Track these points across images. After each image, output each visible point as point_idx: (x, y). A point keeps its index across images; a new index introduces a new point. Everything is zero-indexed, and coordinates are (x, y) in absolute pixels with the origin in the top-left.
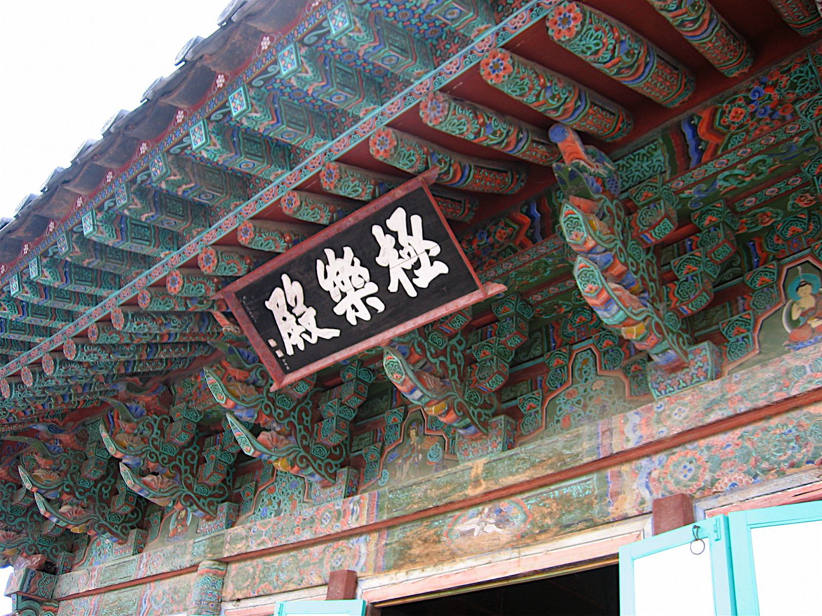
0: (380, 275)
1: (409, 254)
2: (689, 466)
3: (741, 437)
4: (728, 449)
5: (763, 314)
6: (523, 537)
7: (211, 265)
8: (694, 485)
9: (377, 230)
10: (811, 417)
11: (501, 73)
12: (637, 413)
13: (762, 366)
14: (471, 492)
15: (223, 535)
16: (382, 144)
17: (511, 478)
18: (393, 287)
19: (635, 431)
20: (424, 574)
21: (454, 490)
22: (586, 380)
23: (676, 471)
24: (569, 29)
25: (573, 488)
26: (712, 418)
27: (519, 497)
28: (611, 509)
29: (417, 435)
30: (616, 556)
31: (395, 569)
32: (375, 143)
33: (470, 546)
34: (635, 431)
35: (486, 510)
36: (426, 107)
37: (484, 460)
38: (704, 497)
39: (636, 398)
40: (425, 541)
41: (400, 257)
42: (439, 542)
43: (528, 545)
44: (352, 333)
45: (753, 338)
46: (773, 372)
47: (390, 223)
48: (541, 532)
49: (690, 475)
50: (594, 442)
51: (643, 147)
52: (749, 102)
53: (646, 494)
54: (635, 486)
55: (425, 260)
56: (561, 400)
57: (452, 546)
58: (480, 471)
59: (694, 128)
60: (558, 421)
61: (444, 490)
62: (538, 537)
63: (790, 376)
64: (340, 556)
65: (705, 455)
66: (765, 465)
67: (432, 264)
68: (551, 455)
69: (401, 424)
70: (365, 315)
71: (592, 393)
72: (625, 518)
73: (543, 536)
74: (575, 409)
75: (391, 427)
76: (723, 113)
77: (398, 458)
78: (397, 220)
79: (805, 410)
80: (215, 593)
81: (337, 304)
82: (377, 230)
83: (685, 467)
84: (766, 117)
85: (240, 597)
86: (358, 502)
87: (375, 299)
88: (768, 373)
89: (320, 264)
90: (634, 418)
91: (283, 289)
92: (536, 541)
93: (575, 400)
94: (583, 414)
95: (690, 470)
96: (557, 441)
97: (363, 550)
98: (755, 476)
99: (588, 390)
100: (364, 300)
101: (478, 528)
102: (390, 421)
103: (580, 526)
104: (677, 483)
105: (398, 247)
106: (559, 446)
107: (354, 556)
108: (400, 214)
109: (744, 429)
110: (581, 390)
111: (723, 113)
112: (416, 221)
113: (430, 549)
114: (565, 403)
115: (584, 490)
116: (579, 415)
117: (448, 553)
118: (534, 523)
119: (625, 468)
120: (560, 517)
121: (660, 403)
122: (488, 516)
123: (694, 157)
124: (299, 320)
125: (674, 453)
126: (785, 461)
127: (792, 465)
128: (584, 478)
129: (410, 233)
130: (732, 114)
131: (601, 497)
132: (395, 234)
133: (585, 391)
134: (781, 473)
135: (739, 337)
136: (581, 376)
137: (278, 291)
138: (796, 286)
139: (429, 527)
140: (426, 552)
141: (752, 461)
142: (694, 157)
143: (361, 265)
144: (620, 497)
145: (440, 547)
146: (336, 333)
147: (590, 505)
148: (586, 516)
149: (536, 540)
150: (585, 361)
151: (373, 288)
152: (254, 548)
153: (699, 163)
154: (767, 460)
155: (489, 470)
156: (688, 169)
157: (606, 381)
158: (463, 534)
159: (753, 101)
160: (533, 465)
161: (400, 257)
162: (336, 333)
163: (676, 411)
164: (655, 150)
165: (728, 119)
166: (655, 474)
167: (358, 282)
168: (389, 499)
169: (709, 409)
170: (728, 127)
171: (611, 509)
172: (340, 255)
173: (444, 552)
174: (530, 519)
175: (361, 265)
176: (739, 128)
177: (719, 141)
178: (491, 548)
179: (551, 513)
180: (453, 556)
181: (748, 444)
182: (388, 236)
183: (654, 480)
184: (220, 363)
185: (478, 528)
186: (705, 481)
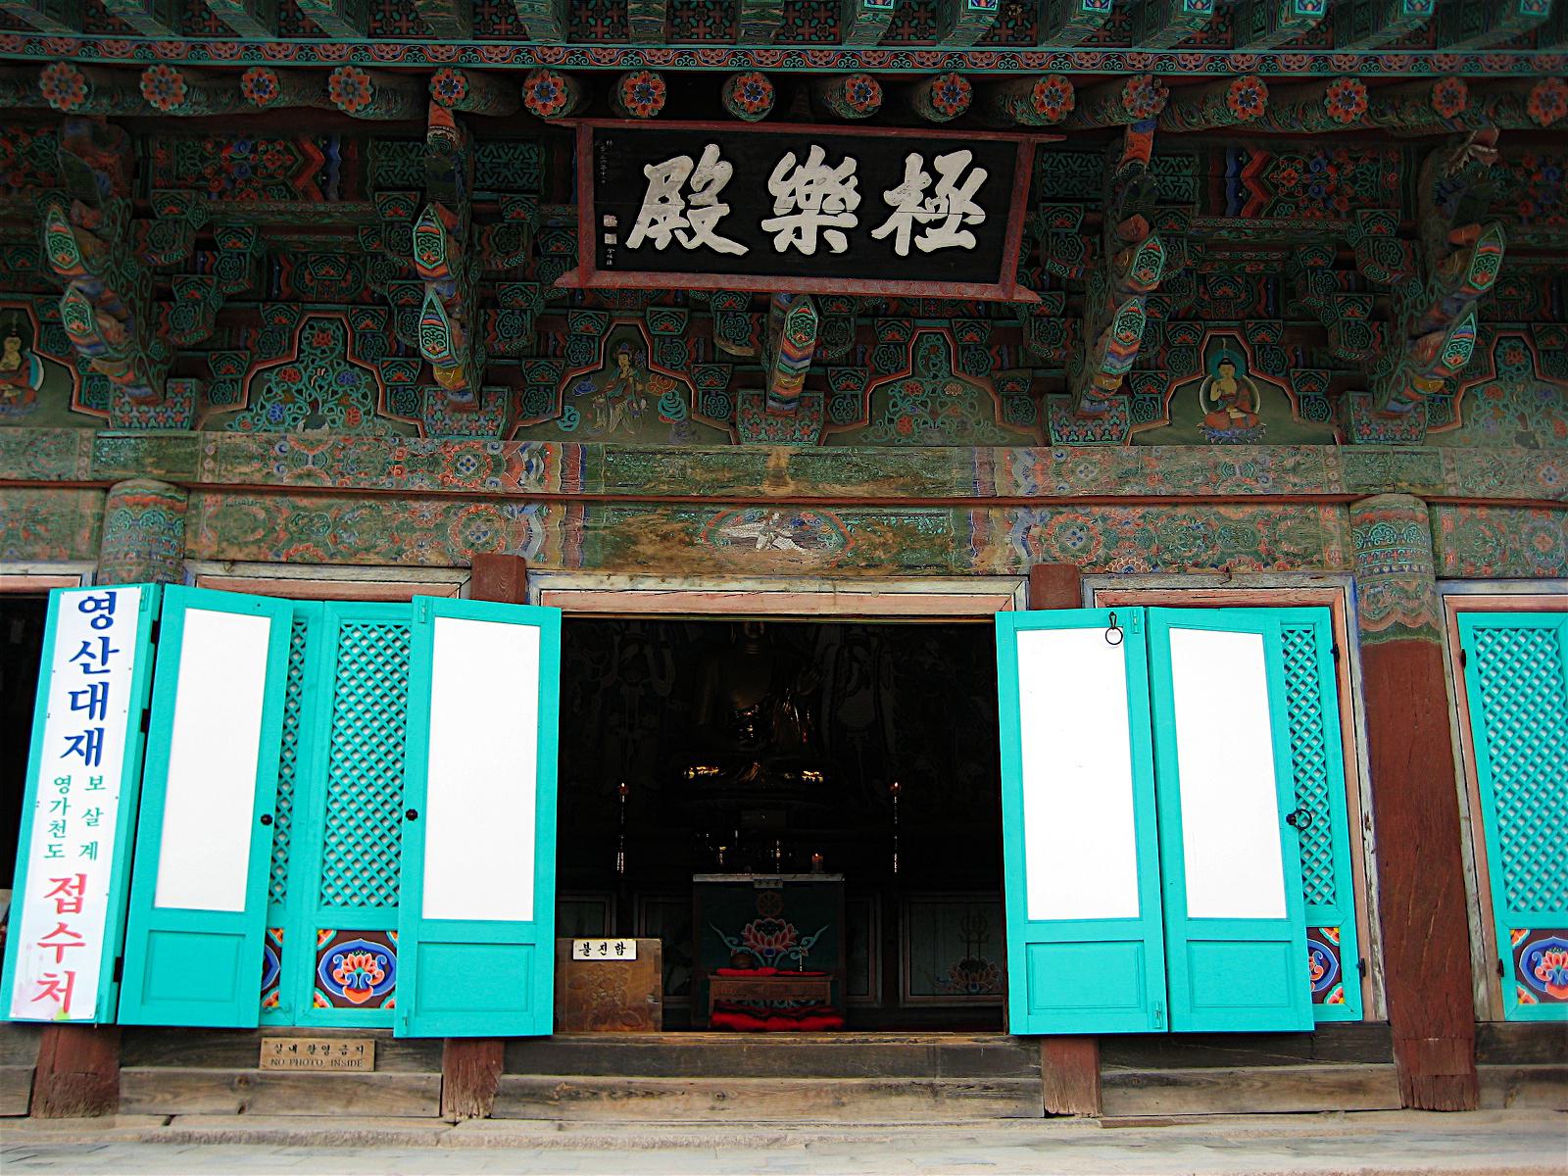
0: (873, 211)
1: (937, 208)
2: (1079, 534)
3: (1143, 517)
4: (1127, 527)
5: (1180, 379)
6: (840, 566)
7: (650, 105)
8: (1085, 558)
9: (914, 161)
10: (1220, 518)
11: (1250, 110)
12: (1029, 454)
13: (1188, 449)
14: (767, 489)
15: (195, 440)
16: (1051, 97)
17: (838, 487)
18: (879, 233)
19: (1027, 477)
20: (665, 586)
21: (737, 479)
22: (935, 376)
23: (1067, 537)
24: (1347, 112)
25: (921, 519)
26: (1127, 490)
27: (833, 512)
28: (973, 560)
29: (632, 365)
30: (992, 617)
31: (607, 568)
32: (1042, 92)
33: (749, 561)
34: (1027, 477)
35: (776, 516)
36: (1136, 88)
37: (792, 448)
38: (1093, 573)
39: (1007, 426)
40: (665, 537)
41: (922, 204)
42: (693, 544)
43: (846, 579)
44: (763, 257)
45: (1163, 404)
46: (1200, 460)
47: (940, 162)
48: (868, 566)
49: (1080, 544)
50: (967, 473)
51: (1174, 156)
52: (1307, 170)
53: (1022, 553)
54: (1007, 540)
55: (954, 222)
56: (896, 391)
57: (717, 555)
58: (783, 463)
59: (1240, 166)
60: (891, 421)
61: (719, 476)
62: (864, 572)
63: (1219, 472)
64: (484, 528)
65: (1100, 526)
66: (1167, 557)
67: (958, 231)
68: (902, 472)
69: (601, 338)
70: (808, 246)
71: (944, 398)
72: (992, 575)
73: (872, 572)
74: (918, 411)
75: (579, 338)
76: (1277, 167)
77: (598, 393)
78: (951, 164)
79: (1215, 509)
80: (174, 542)
81: (774, 216)
82: (914, 161)
83: (1074, 533)
84: (1319, 198)
85: (240, 556)
86: (541, 452)
87: (842, 236)
88: (1194, 458)
89: (790, 159)
90: (1024, 458)
91: (696, 163)
92: (860, 577)
93: (920, 399)
94: (931, 423)
95: (1080, 539)
96: (911, 456)
97: (537, 527)
98: (1155, 566)
99: (939, 391)
100: (821, 229)
101: (762, 540)
102: (580, 327)
103: (928, 571)
104: (1064, 550)
105: (929, 192)
106: (916, 462)
107: (519, 534)
108: (964, 157)
109: (1147, 509)
110: (929, 388)
111: (1277, 167)
112: (979, 176)
113: (674, 552)
114: (903, 398)
115: (937, 527)
116: (925, 423)
117: (711, 563)
118: (857, 552)
119: (994, 513)
120: (899, 553)
121: (1061, 451)
122: (779, 524)
123: (1232, 204)
124: (690, 212)
125: (1061, 513)
126: (1189, 558)
127: (1196, 565)
128: (935, 511)
129: (959, 184)
130: (1285, 174)
131: (962, 542)
132: (936, 177)
133: (934, 391)
134: (1182, 570)
135: (1148, 397)
136: (926, 366)
137: (686, 161)
138: (1219, 360)
139: (670, 519)
140: (667, 553)
141: (1154, 548)
142: (1232, 204)
143: (856, 189)
144: (987, 548)
145: (694, 552)
146: (740, 249)
147: (944, 549)
148: (938, 560)
149: (859, 575)
150: (935, 349)
151: (851, 221)
152: (287, 481)
153: (1237, 214)
154: (1171, 551)
155: (799, 466)
156: (1223, 215)
157: (964, 388)
158: (736, 542)
159: (1309, 172)
160: (874, 478)
161: (922, 204)
162: (740, 249)
163: (1082, 468)
164: (1187, 167)
165: (1278, 176)
166: (1034, 531)
167: (831, 205)
168: (609, 464)
169: (1124, 478)
170: (1276, 187)
171: (973, 560)
172: (833, 161)
173: (701, 560)
174: (851, 545)
175: (856, 189)
176: (1287, 195)
177: (1265, 200)
178: (785, 571)
179: (884, 544)
180: (719, 570)
181: (1150, 528)
182: (925, 174)
183: (1033, 538)
184: (295, 141)
185: (762, 540)
186: (1098, 557)
